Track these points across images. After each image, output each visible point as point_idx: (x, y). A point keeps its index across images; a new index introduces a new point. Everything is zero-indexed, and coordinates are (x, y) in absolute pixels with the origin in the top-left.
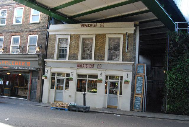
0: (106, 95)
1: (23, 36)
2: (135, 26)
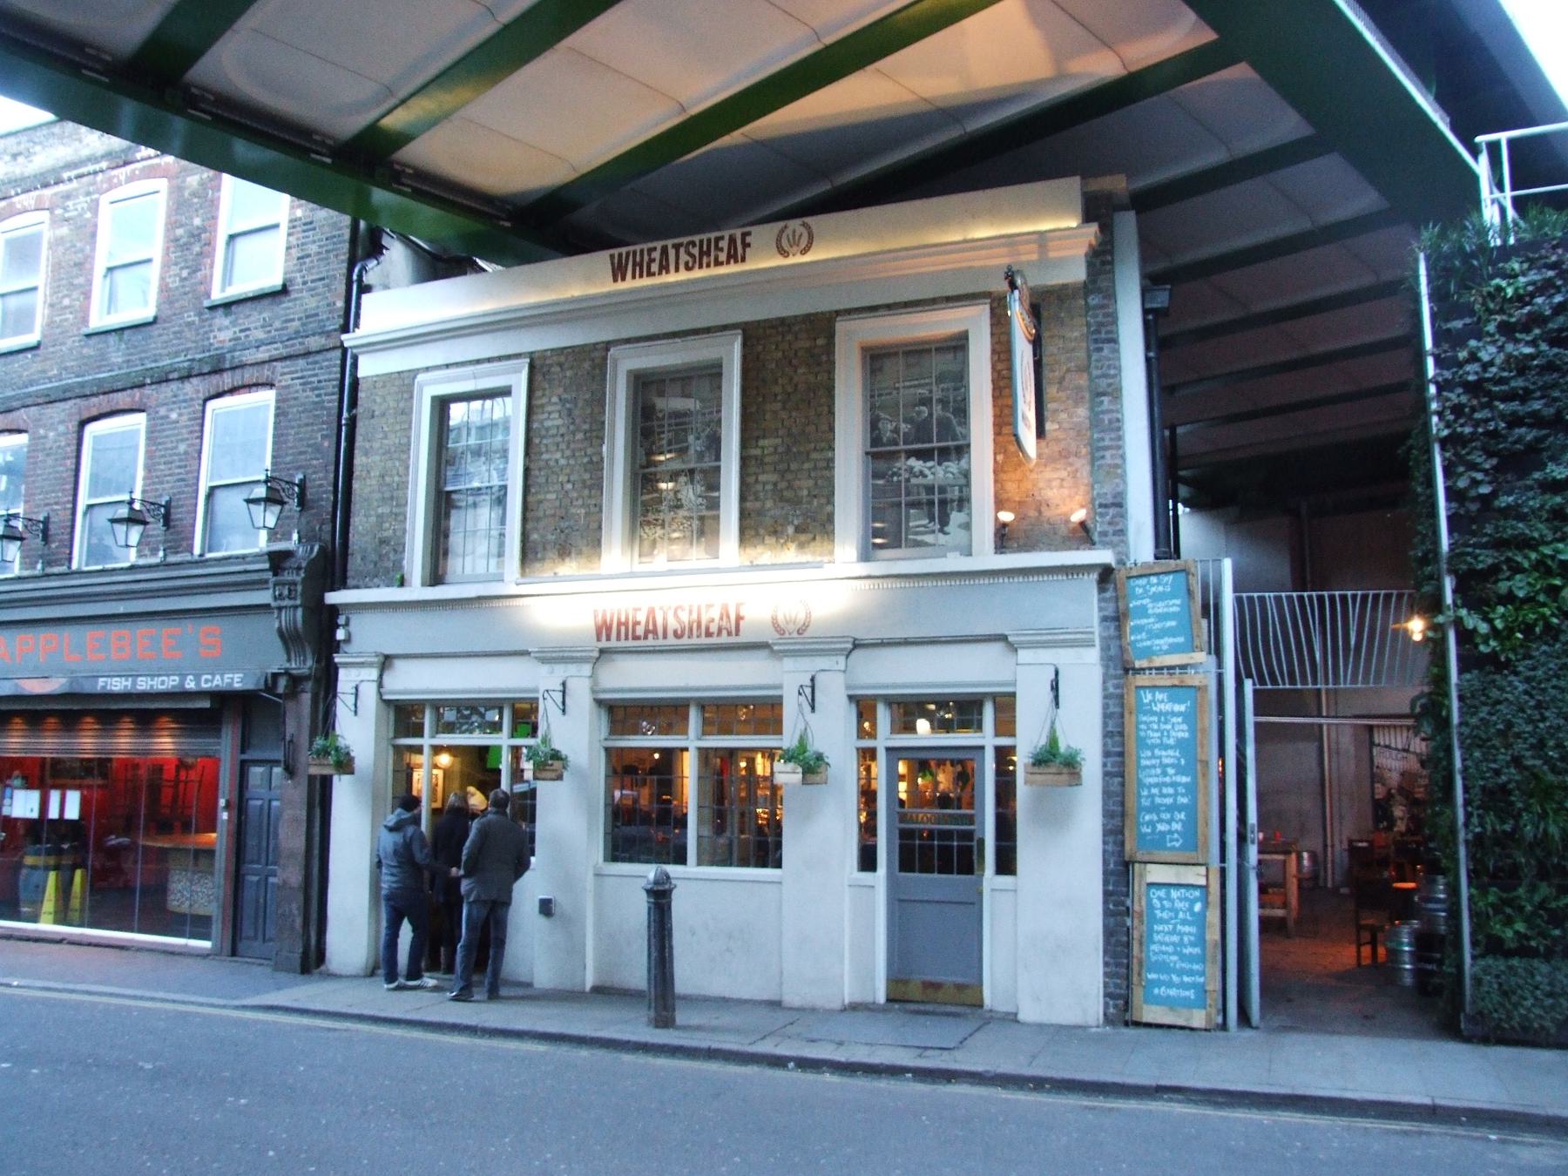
0: (867, 877)
1: (163, 411)
2: (1095, 210)
